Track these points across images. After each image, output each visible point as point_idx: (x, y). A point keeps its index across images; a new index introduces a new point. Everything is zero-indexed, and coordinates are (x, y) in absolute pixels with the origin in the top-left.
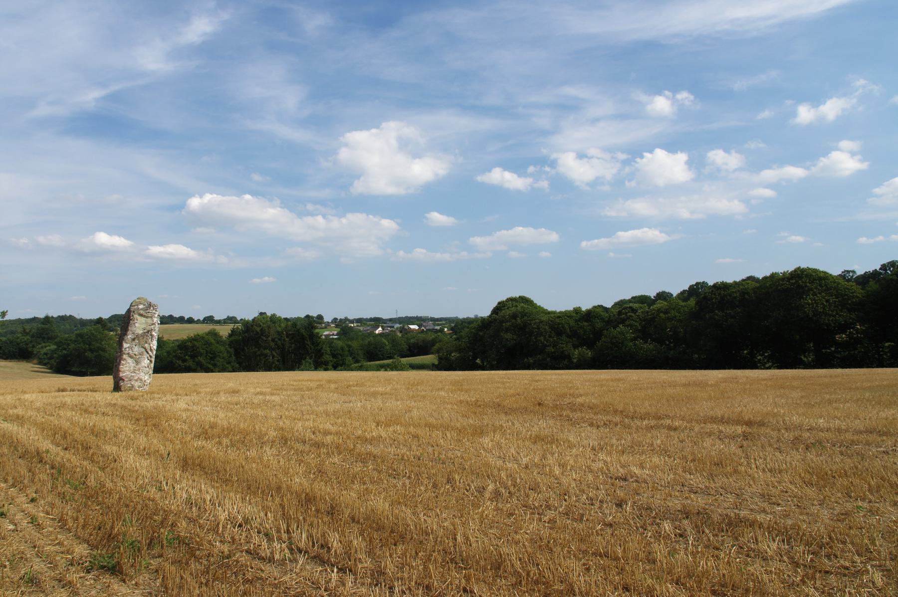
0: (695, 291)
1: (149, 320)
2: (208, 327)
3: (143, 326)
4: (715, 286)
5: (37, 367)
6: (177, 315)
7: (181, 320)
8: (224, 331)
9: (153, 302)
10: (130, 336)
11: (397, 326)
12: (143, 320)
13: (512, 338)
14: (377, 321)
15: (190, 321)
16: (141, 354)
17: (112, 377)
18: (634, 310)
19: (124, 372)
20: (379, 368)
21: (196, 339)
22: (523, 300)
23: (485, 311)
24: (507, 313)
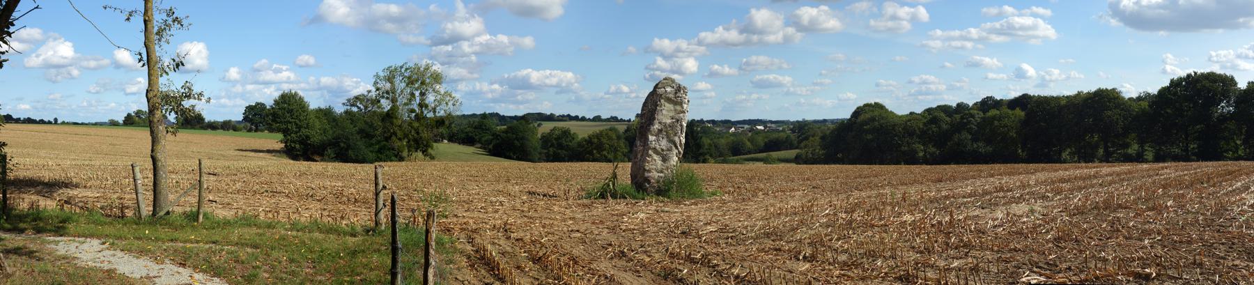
0: (1023, 101)
1: (678, 108)
2: (607, 126)
3: (672, 114)
4: (1160, 92)
5: (481, 151)
6: (573, 115)
7: (576, 118)
8: (622, 128)
9: (683, 84)
10: (656, 126)
11: (746, 126)
12: (671, 106)
13: (868, 139)
14: (728, 123)
15: (583, 119)
16: (670, 150)
17: (240, 118)
18: (972, 116)
19: (649, 171)
20: (737, 162)
21: (598, 136)
22: (878, 106)
23: (846, 114)
24: (862, 118)
